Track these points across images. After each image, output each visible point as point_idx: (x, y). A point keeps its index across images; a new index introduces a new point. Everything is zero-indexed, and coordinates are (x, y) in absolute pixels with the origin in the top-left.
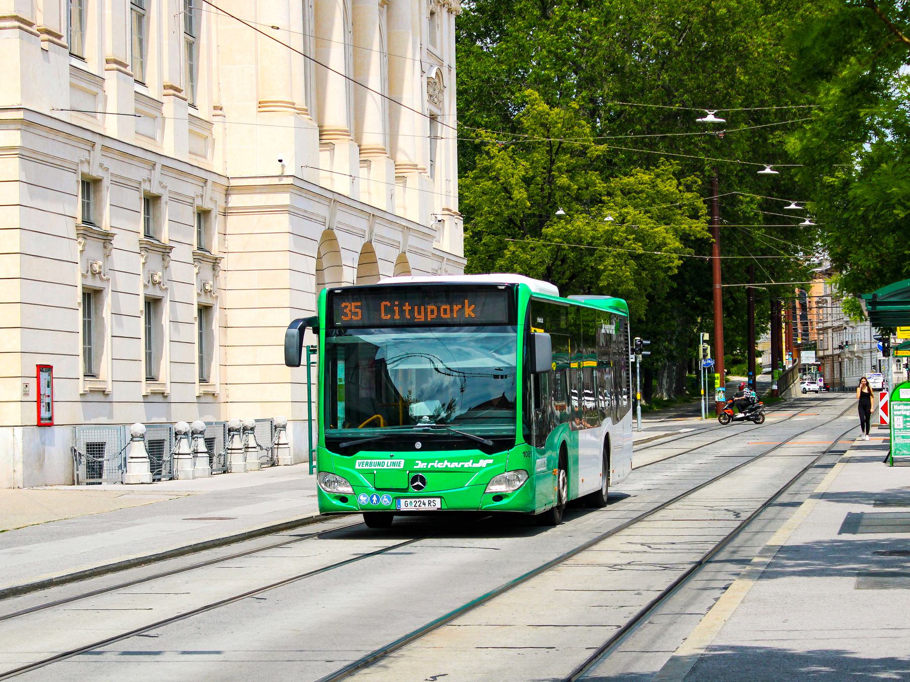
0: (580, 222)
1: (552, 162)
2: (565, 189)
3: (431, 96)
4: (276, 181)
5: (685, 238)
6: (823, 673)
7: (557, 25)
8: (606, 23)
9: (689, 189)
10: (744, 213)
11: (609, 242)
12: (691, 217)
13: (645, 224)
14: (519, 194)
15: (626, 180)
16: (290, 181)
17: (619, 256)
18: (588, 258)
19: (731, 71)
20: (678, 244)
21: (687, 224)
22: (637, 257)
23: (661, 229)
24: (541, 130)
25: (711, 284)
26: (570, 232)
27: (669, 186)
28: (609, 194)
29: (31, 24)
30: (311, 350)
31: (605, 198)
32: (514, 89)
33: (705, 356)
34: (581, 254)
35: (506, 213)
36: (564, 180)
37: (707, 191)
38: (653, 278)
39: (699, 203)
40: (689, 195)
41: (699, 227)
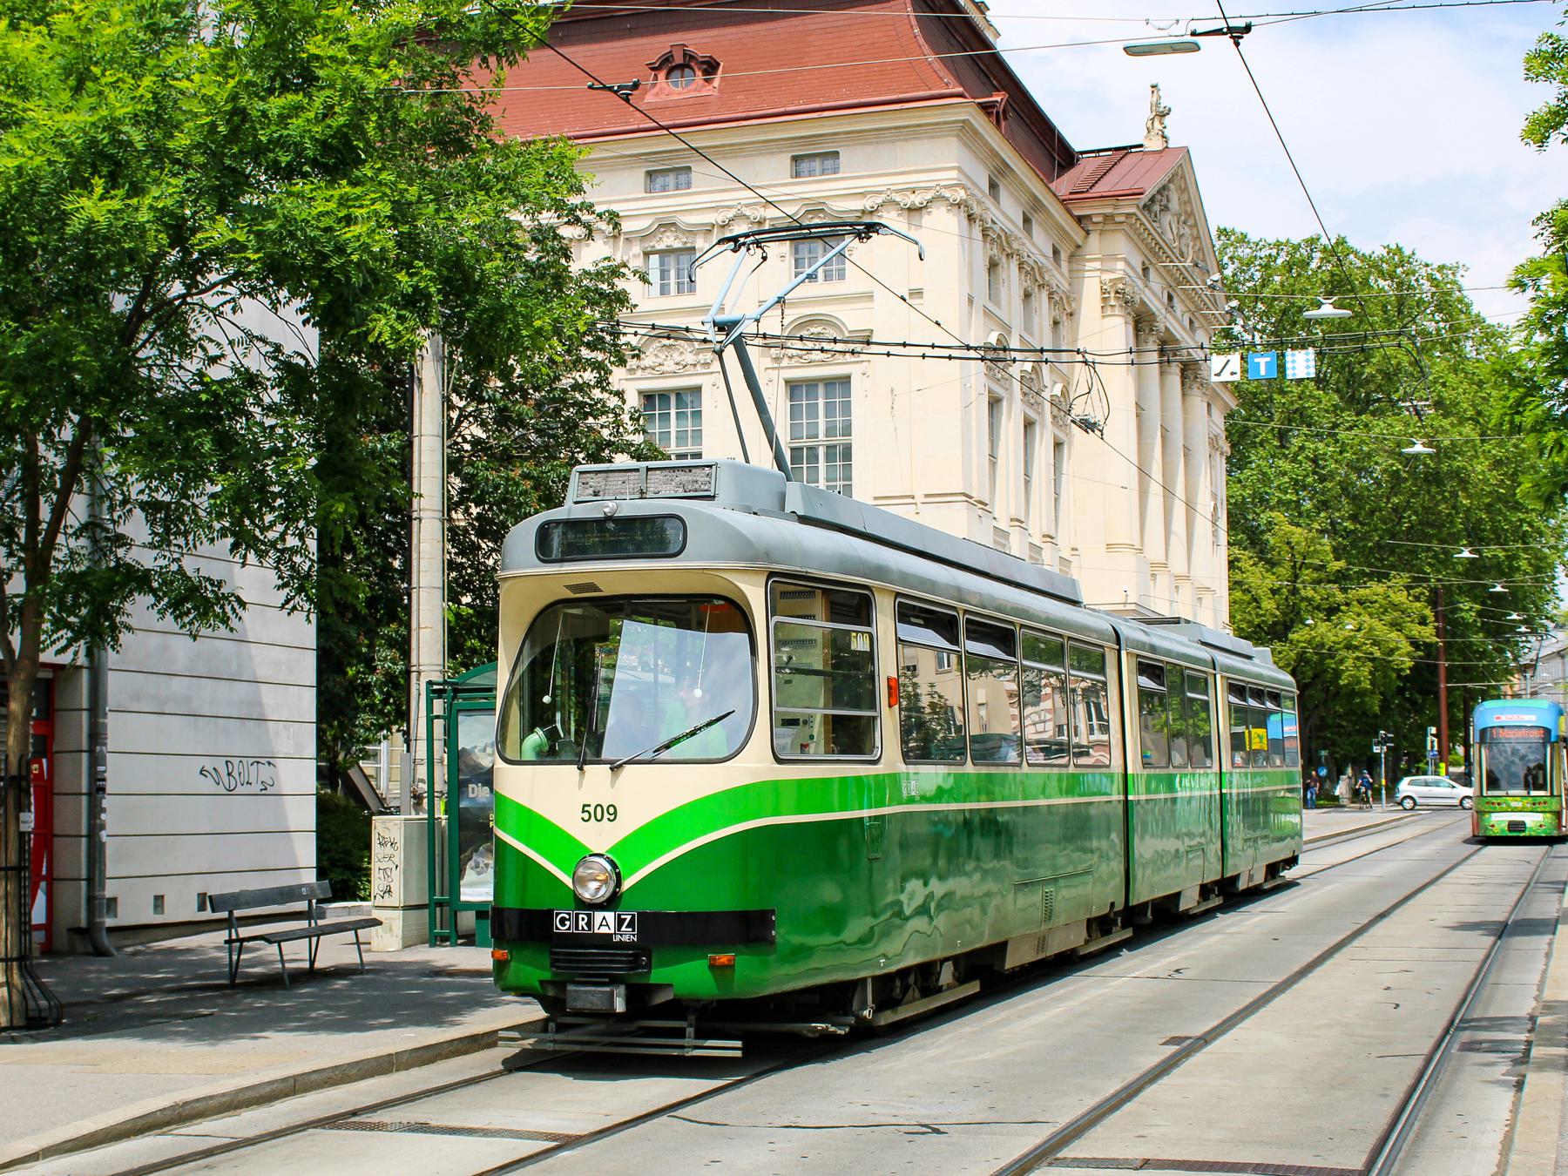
0: (1323, 627)
1: (1296, 576)
2: (1309, 600)
3: (1025, 394)
4: (1121, 607)
5: (1415, 644)
6: (1521, 734)
7: (1296, 455)
8: (1341, 453)
9: (1417, 599)
10: (1463, 618)
11: (1349, 647)
12: (1420, 624)
13: (1380, 629)
14: (1269, 605)
15: (1362, 592)
16: (1133, 607)
17: (1358, 658)
18: (1328, 661)
19: (1454, 495)
20: (1411, 649)
21: (1415, 630)
22: (1373, 660)
23: (1394, 635)
24: (1286, 548)
25: (1436, 684)
26: (1314, 638)
27: (1400, 597)
28: (1347, 604)
29: (971, 497)
30: (435, 691)
31: (1343, 608)
32: (1257, 511)
33: (1432, 747)
34: (1323, 657)
35: (1257, 621)
36: (1310, 593)
37: (1433, 602)
38: (1386, 676)
39: (1428, 612)
40: (1418, 604)
41: (1428, 633)
